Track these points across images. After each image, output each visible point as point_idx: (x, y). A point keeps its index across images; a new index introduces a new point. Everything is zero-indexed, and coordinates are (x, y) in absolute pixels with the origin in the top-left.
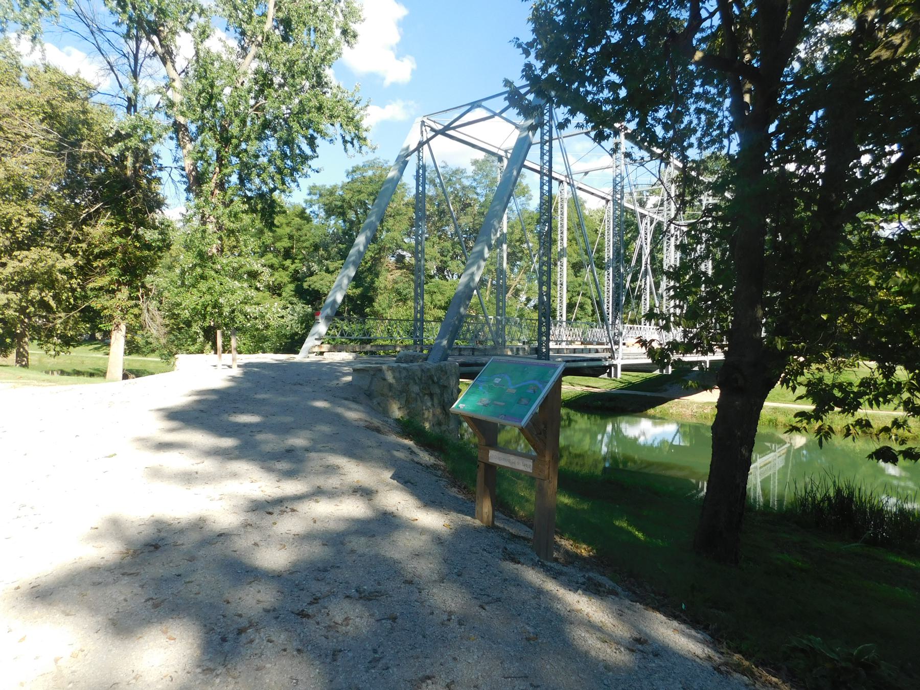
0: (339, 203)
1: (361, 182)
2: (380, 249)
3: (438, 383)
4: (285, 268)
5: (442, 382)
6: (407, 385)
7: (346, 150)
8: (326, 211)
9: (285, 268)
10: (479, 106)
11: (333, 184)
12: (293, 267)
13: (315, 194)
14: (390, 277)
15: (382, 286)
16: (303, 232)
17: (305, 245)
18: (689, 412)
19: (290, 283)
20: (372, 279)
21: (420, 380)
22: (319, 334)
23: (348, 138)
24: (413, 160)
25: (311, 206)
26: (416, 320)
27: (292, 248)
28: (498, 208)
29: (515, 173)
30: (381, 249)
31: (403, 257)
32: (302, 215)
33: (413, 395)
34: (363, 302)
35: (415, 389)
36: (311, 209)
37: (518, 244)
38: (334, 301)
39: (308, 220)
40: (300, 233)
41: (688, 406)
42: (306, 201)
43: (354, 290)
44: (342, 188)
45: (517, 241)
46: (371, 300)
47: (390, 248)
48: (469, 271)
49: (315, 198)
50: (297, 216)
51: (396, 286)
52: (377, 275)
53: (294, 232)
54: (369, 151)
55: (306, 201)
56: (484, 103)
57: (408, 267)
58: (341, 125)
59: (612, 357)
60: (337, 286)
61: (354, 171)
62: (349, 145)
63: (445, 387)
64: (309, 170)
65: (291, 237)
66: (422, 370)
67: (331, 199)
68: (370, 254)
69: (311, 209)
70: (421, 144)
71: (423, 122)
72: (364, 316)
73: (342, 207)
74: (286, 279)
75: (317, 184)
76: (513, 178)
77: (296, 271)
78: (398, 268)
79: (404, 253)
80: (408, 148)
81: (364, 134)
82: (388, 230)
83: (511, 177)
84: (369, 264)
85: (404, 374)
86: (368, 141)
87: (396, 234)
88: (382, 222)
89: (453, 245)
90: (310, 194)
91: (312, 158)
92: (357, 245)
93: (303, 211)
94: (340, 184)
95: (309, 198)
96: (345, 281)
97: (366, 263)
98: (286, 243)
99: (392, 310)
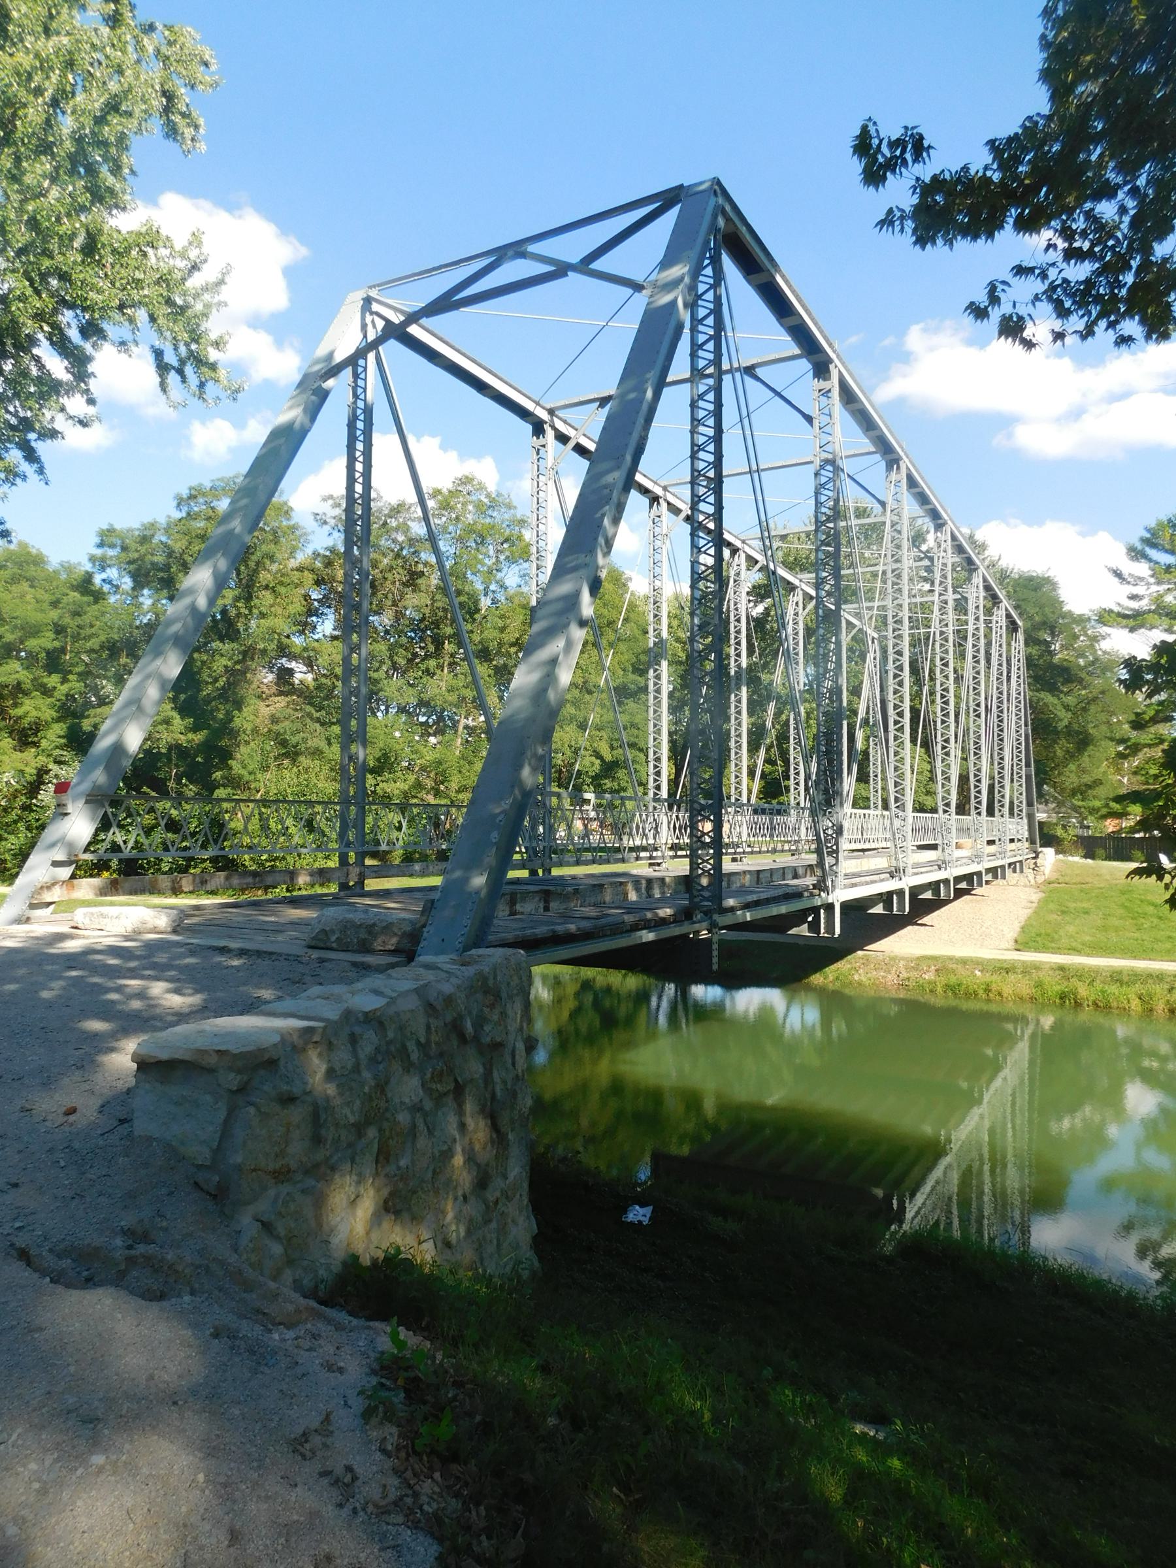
0: (159, 559)
1: (209, 519)
2: (245, 653)
3: (476, 1038)
4: (46, 692)
5: (490, 1033)
6: (381, 1087)
7: (163, 386)
8: (135, 576)
9: (46, 692)
10: (523, 255)
11: (147, 519)
12: (64, 689)
13: (112, 546)
14: (265, 711)
15: (248, 727)
16: (86, 619)
17: (89, 645)
18: (891, 978)
19: (58, 720)
20: (228, 713)
21: (423, 1047)
22: (70, 846)
23: (170, 358)
24: (339, 386)
25: (103, 569)
26: (345, 801)
27: (63, 650)
28: (610, 478)
29: (649, 394)
30: (248, 653)
31: (290, 672)
32: (85, 585)
33: (403, 1118)
34: (208, 760)
35: (408, 1088)
36: (104, 576)
37: (513, 650)
38: (118, 749)
39: (98, 597)
40: (78, 621)
41: (890, 962)
42: (92, 559)
43: (190, 736)
44: (167, 530)
45: (512, 645)
46: (226, 756)
47: (264, 652)
48: (544, 654)
49: (111, 552)
50: (74, 588)
51: (275, 728)
52: (239, 705)
53: (67, 620)
54: (223, 395)
55: (92, 559)
56: (532, 248)
57: (303, 693)
58: (153, 319)
59: (821, 886)
60: (128, 704)
61: (192, 497)
62: (173, 378)
63: (497, 1046)
64: (60, 417)
65: (59, 630)
66: (430, 1009)
67: (143, 550)
68: (224, 661)
69: (104, 576)
70: (361, 353)
71: (368, 301)
72: (211, 787)
73: (167, 567)
74: (48, 714)
75: (118, 526)
76: (645, 407)
77: (70, 697)
78: (281, 693)
79: (293, 665)
80: (331, 355)
81: (213, 355)
82: (263, 616)
83: (641, 400)
84: (221, 683)
85: (370, 1041)
86: (222, 373)
87: (282, 625)
88: (249, 598)
89: (391, 648)
90: (101, 545)
91: (70, 390)
92: (191, 591)
93: (88, 578)
94: (162, 520)
95: (98, 552)
96: (153, 692)
97: (216, 680)
98: (47, 641)
99: (268, 775)
